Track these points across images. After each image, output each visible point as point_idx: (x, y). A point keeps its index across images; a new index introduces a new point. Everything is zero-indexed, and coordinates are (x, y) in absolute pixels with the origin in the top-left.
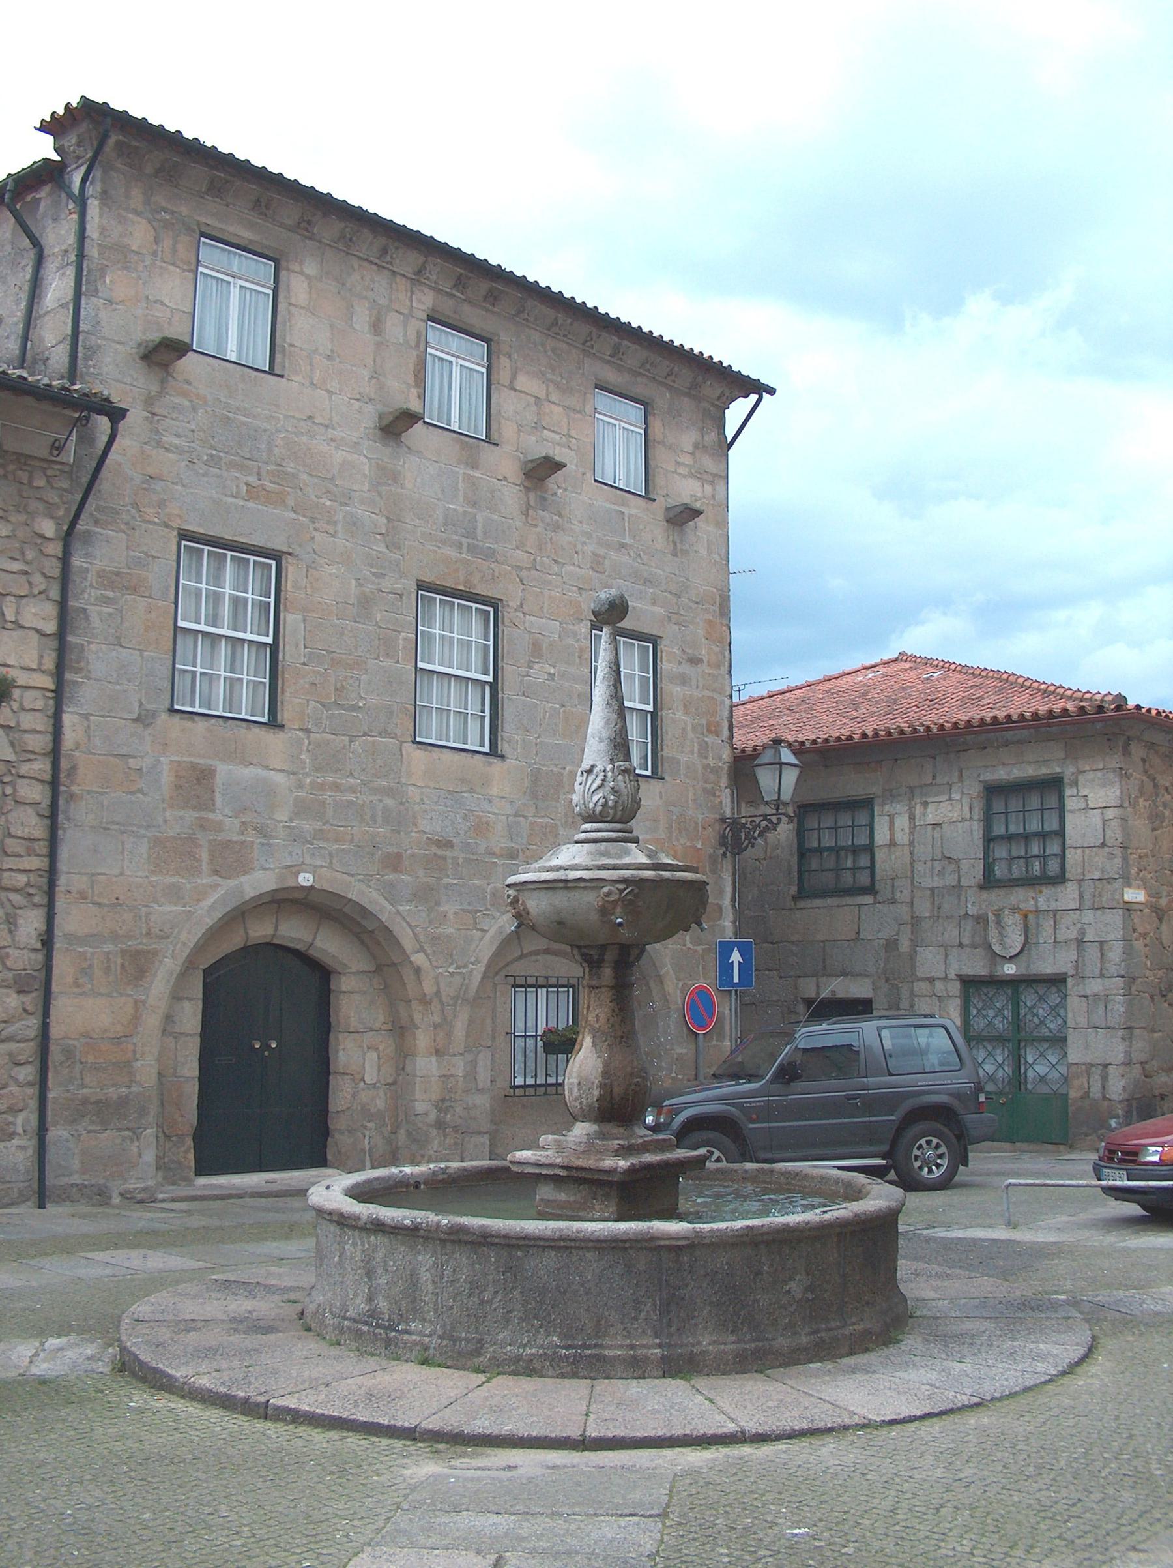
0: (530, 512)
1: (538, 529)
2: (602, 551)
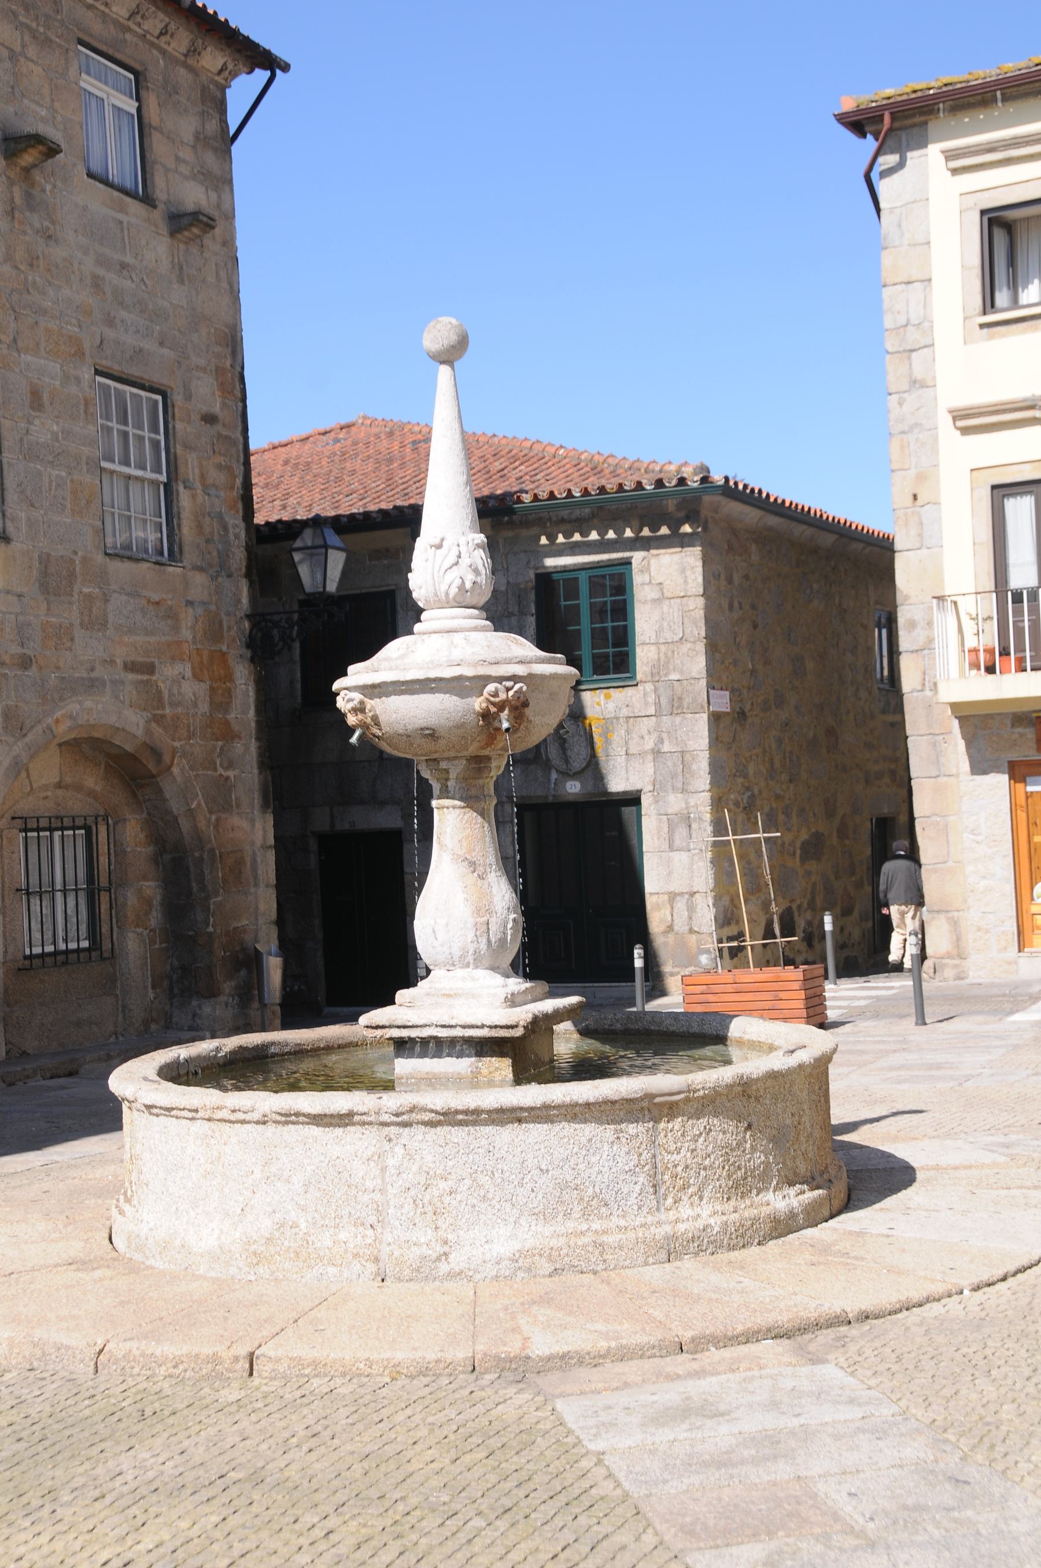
0: (17, 214)
1: (27, 238)
2: (101, 272)
